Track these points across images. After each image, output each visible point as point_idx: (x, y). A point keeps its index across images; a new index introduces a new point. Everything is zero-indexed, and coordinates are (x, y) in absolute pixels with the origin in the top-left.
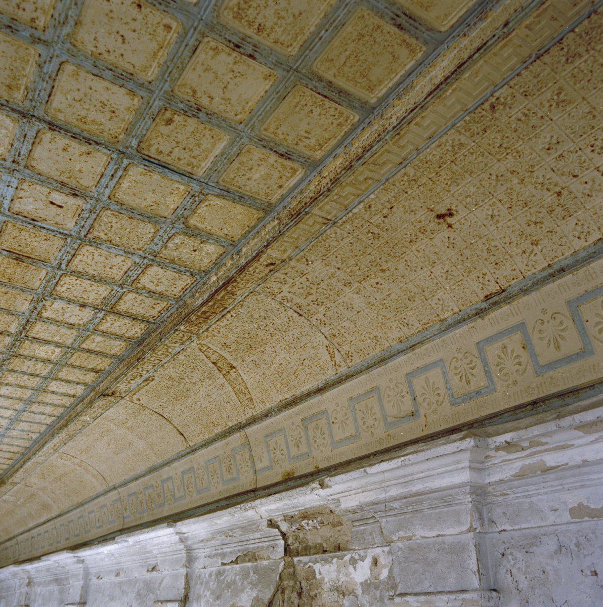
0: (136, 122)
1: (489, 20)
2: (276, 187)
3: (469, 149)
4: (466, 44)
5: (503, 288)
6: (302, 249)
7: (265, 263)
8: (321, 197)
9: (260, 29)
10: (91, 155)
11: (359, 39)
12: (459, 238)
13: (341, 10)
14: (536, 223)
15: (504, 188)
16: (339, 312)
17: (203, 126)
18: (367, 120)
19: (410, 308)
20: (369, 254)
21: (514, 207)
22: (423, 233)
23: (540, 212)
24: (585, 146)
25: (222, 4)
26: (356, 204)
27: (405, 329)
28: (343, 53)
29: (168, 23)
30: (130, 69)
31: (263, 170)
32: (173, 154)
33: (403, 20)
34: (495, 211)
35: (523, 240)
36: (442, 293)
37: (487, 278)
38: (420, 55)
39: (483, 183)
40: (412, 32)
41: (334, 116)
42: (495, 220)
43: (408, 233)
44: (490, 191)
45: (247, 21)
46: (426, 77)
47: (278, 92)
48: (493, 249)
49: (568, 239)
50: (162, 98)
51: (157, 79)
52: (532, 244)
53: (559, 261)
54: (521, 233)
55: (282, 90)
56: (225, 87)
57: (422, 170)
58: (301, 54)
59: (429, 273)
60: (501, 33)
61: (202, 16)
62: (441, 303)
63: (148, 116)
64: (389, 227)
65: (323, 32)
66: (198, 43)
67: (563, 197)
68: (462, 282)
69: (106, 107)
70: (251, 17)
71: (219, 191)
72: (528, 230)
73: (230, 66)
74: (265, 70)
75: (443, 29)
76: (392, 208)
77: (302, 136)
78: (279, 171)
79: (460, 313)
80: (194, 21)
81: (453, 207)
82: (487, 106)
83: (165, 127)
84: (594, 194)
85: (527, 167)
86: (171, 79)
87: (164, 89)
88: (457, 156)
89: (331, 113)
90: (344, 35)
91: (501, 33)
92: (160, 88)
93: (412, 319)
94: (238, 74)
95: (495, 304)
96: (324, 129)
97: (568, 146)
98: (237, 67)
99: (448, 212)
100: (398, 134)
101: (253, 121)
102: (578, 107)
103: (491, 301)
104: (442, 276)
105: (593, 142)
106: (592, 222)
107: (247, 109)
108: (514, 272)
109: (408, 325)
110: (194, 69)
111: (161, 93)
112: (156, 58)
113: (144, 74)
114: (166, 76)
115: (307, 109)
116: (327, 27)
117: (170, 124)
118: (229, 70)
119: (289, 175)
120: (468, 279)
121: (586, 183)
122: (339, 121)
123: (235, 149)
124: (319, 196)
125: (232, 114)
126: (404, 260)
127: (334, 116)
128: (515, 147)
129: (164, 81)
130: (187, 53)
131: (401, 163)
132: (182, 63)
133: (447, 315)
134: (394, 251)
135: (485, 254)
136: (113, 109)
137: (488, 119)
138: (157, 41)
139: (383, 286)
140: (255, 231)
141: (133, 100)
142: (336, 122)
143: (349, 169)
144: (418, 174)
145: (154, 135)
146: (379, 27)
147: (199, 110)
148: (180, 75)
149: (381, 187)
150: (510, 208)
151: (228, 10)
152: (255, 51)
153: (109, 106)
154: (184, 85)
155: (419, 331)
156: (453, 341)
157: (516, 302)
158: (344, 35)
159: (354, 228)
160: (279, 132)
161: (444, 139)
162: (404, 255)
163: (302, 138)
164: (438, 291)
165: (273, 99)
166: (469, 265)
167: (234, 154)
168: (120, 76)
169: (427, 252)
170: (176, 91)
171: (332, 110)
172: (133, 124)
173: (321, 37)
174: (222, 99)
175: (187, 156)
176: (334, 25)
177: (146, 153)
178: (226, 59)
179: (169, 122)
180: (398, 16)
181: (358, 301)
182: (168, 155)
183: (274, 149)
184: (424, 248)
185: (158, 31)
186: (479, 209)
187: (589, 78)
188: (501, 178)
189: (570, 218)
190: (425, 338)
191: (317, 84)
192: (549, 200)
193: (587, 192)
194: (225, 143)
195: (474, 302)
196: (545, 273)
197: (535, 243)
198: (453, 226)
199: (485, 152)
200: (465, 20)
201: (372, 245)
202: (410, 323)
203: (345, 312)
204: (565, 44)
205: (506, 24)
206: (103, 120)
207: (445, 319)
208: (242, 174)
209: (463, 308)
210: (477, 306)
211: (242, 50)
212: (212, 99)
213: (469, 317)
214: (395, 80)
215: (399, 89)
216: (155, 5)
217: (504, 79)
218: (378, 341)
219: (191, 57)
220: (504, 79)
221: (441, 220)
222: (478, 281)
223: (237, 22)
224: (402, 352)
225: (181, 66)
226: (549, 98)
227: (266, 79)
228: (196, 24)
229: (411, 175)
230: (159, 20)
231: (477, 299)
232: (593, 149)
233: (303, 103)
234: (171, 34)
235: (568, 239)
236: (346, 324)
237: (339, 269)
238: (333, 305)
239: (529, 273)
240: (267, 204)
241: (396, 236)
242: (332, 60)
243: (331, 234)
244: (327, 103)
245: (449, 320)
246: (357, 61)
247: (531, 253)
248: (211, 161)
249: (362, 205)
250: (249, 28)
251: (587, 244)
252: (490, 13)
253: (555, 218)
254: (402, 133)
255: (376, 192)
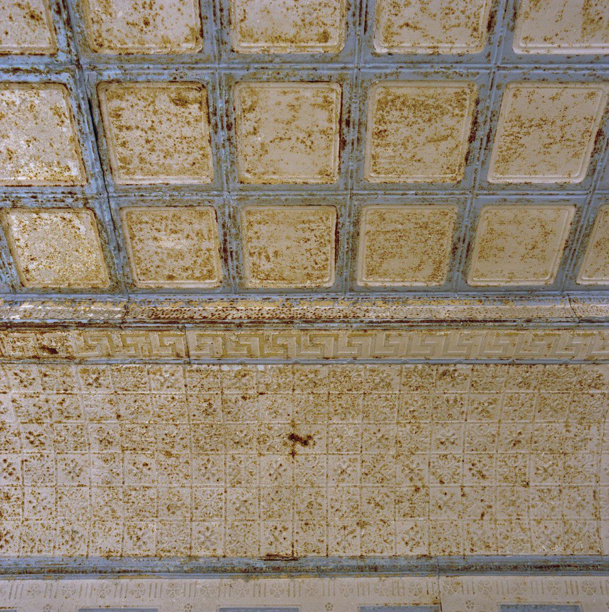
0: (151, 61)
1: (508, 307)
2: (166, 273)
3: (388, 394)
4: (480, 310)
5: (295, 555)
6: (110, 362)
7: (45, 343)
8: (222, 325)
9: (380, 134)
10: (33, 22)
11: (421, 227)
12: (291, 473)
13: (444, 193)
14: (377, 505)
15: (377, 452)
16: (51, 471)
17: (205, 143)
18: (333, 295)
19: (160, 518)
20: (176, 425)
21: (369, 476)
22: (259, 443)
23: (388, 496)
24: (469, 461)
25: (391, 81)
26: (237, 362)
27: (129, 544)
28: (397, 223)
29: (331, 35)
30: (237, 16)
31: (183, 245)
32: (129, 133)
33: (462, 247)
34: (350, 468)
35: (351, 514)
36: (218, 523)
37: (284, 534)
38: (434, 284)
39: (365, 434)
40: (454, 263)
41: (316, 264)
42: (342, 477)
43: (245, 433)
44: (363, 445)
45: (382, 116)
46: (424, 305)
47: (313, 195)
48: (316, 506)
49: (396, 539)
50: (217, 76)
51: (244, 57)
52: (358, 524)
53: (375, 557)
54: (356, 506)
55: (318, 197)
56: (281, 139)
57: (333, 380)
58: (376, 188)
59: (222, 490)
60: (520, 324)
61: (364, 67)
62: (208, 534)
63: (174, 71)
64: (235, 411)
65: (413, 192)
66: (327, 80)
67: (418, 495)
68: (251, 522)
69: (147, 11)
70: (389, 118)
71: (107, 218)
72: (365, 507)
73: (315, 129)
74: (333, 164)
75: (469, 282)
76: (261, 394)
77: (266, 252)
78: (195, 262)
79: (222, 559)
80: (352, 63)
81: (315, 438)
82: (442, 369)
83: (168, 99)
84: (444, 509)
85: (413, 446)
86: (255, 74)
87: (233, 72)
88: (374, 392)
89: (318, 260)
90: (418, 211)
91: (520, 324)
92: (231, 66)
93: (150, 534)
94: (309, 143)
95: (277, 570)
96: (292, 266)
97: (457, 451)
98: (318, 135)
99: (306, 439)
100: (365, 331)
101: (253, 193)
102: (491, 425)
103: (272, 563)
104: (234, 503)
105: (476, 462)
106: (427, 535)
107: (266, 177)
108: (319, 544)
109: (139, 539)
110: (285, 93)
111: (223, 72)
112: (273, 42)
113: (239, 37)
114: (256, 66)
115: (308, 234)
116: (420, 192)
117: (177, 105)
118: (309, 130)
119: (197, 274)
120: (262, 524)
121: (446, 494)
122: (313, 272)
123: (195, 198)
124: (220, 323)
125: (247, 166)
126: (207, 457)
127: (316, 264)
128: (421, 421)
129: (246, 66)
130: (305, 74)
131: (327, 358)
132: (288, 75)
133: (202, 553)
134: (208, 441)
135: (302, 507)
136: (152, 21)
137: (431, 380)
138: (298, 33)
139: (149, 472)
140: (73, 296)
141: (187, 40)
142: (309, 270)
143: (285, 323)
144: (325, 381)
145: (144, 93)
146: (442, 234)
147: (229, 127)
148: (268, 81)
149: (280, 366)
150: (366, 474)
151: (384, 90)
152: (353, 144)
153: (153, 13)
154: (253, 92)
155: (148, 556)
156: (188, 590)
157: (300, 580)
158: (418, 211)
159: (199, 385)
160: (256, 227)
161: (382, 368)
162: (213, 452)
163: (264, 254)
164: (216, 518)
165: (300, 195)
166: (275, 509)
167: (187, 201)
168: (218, 7)
169: (242, 466)
170: (238, 88)
171: (324, 257)
172: (145, 58)
173: (406, 194)
174: (262, 144)
175: (137, 150)
176: (426, 197)
177: (103, 97)
178: (326, 120)
179: (181, 102)
180: (464, 240)
181: (95, 471)
182: (120, 128)
183: (228, 238)
184: (242, 459)
185: (313, 28)
186: (338, 456)
187: (517, 408)
188: (384, 441)
189: (409, 519)
190: (150, 569)
191: (348, 224)
192: (405, 489)
193: (441, 503)
194: (196, 182)
195: (249, 554)
196: (354, 563)
197: (362, 525)
198: (295, 456)
199: (397, 407)
200: (488, 291)
201: (192, 418)
202: (144, 539)
203: (61, 475)
204: (532, 370)
205: (529, 321)
206: (120, 14)
207: (196, 558)
208: (159, 227)
209: (229, 554)
210: (251, 562)
211: (345, 130)
212: (255, 134)
213: (233, 570)
214: (396, 284)
215: (388, 295)
216: (349, 9)
217: (477, 359)
218: (73, 539)
219: (302, 81)
220: (477, 359)
221: (290, 443)
222: (272, 532)
223: (376, 107)
224: (100, 572)
225: (281, 76)
226: (482, 401)
227: (320, 173)
228: (351, 66)
229: (319, 377)
230: (328, 22)
231: (256, 553)
232: (472, 467)
233: (313, 226)
234: (318, 45)
235: (396, 539)
236: (46, 492)
237: (119, 416)
238: (52, 456)
239: (335, 554)
240: (130, 281)
241: (228, 426)
242: (384, 219)
243: (166, 372)
244: (330, 249)
245: (201, 561)
246: (397, 241)
247: (352, 532)
248: (153, 182)
249: (240, 367)
250: (375, 123)
251: (410, 554)
252: (511, 303)
253: (397, 511)
254: (369, 332)
255: (270, 366)
